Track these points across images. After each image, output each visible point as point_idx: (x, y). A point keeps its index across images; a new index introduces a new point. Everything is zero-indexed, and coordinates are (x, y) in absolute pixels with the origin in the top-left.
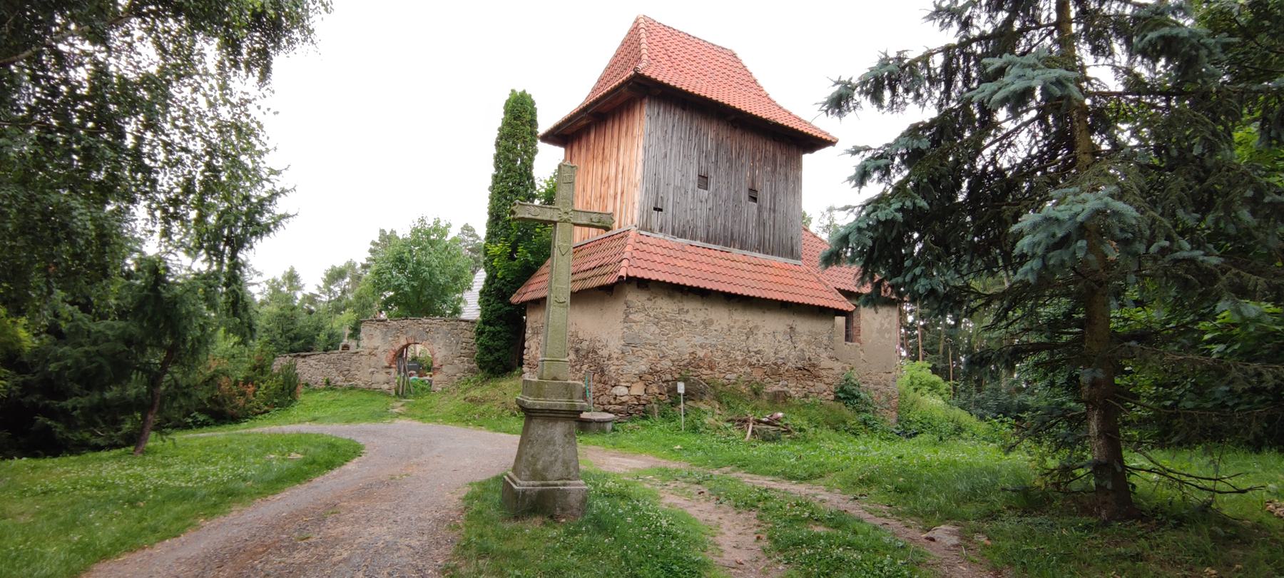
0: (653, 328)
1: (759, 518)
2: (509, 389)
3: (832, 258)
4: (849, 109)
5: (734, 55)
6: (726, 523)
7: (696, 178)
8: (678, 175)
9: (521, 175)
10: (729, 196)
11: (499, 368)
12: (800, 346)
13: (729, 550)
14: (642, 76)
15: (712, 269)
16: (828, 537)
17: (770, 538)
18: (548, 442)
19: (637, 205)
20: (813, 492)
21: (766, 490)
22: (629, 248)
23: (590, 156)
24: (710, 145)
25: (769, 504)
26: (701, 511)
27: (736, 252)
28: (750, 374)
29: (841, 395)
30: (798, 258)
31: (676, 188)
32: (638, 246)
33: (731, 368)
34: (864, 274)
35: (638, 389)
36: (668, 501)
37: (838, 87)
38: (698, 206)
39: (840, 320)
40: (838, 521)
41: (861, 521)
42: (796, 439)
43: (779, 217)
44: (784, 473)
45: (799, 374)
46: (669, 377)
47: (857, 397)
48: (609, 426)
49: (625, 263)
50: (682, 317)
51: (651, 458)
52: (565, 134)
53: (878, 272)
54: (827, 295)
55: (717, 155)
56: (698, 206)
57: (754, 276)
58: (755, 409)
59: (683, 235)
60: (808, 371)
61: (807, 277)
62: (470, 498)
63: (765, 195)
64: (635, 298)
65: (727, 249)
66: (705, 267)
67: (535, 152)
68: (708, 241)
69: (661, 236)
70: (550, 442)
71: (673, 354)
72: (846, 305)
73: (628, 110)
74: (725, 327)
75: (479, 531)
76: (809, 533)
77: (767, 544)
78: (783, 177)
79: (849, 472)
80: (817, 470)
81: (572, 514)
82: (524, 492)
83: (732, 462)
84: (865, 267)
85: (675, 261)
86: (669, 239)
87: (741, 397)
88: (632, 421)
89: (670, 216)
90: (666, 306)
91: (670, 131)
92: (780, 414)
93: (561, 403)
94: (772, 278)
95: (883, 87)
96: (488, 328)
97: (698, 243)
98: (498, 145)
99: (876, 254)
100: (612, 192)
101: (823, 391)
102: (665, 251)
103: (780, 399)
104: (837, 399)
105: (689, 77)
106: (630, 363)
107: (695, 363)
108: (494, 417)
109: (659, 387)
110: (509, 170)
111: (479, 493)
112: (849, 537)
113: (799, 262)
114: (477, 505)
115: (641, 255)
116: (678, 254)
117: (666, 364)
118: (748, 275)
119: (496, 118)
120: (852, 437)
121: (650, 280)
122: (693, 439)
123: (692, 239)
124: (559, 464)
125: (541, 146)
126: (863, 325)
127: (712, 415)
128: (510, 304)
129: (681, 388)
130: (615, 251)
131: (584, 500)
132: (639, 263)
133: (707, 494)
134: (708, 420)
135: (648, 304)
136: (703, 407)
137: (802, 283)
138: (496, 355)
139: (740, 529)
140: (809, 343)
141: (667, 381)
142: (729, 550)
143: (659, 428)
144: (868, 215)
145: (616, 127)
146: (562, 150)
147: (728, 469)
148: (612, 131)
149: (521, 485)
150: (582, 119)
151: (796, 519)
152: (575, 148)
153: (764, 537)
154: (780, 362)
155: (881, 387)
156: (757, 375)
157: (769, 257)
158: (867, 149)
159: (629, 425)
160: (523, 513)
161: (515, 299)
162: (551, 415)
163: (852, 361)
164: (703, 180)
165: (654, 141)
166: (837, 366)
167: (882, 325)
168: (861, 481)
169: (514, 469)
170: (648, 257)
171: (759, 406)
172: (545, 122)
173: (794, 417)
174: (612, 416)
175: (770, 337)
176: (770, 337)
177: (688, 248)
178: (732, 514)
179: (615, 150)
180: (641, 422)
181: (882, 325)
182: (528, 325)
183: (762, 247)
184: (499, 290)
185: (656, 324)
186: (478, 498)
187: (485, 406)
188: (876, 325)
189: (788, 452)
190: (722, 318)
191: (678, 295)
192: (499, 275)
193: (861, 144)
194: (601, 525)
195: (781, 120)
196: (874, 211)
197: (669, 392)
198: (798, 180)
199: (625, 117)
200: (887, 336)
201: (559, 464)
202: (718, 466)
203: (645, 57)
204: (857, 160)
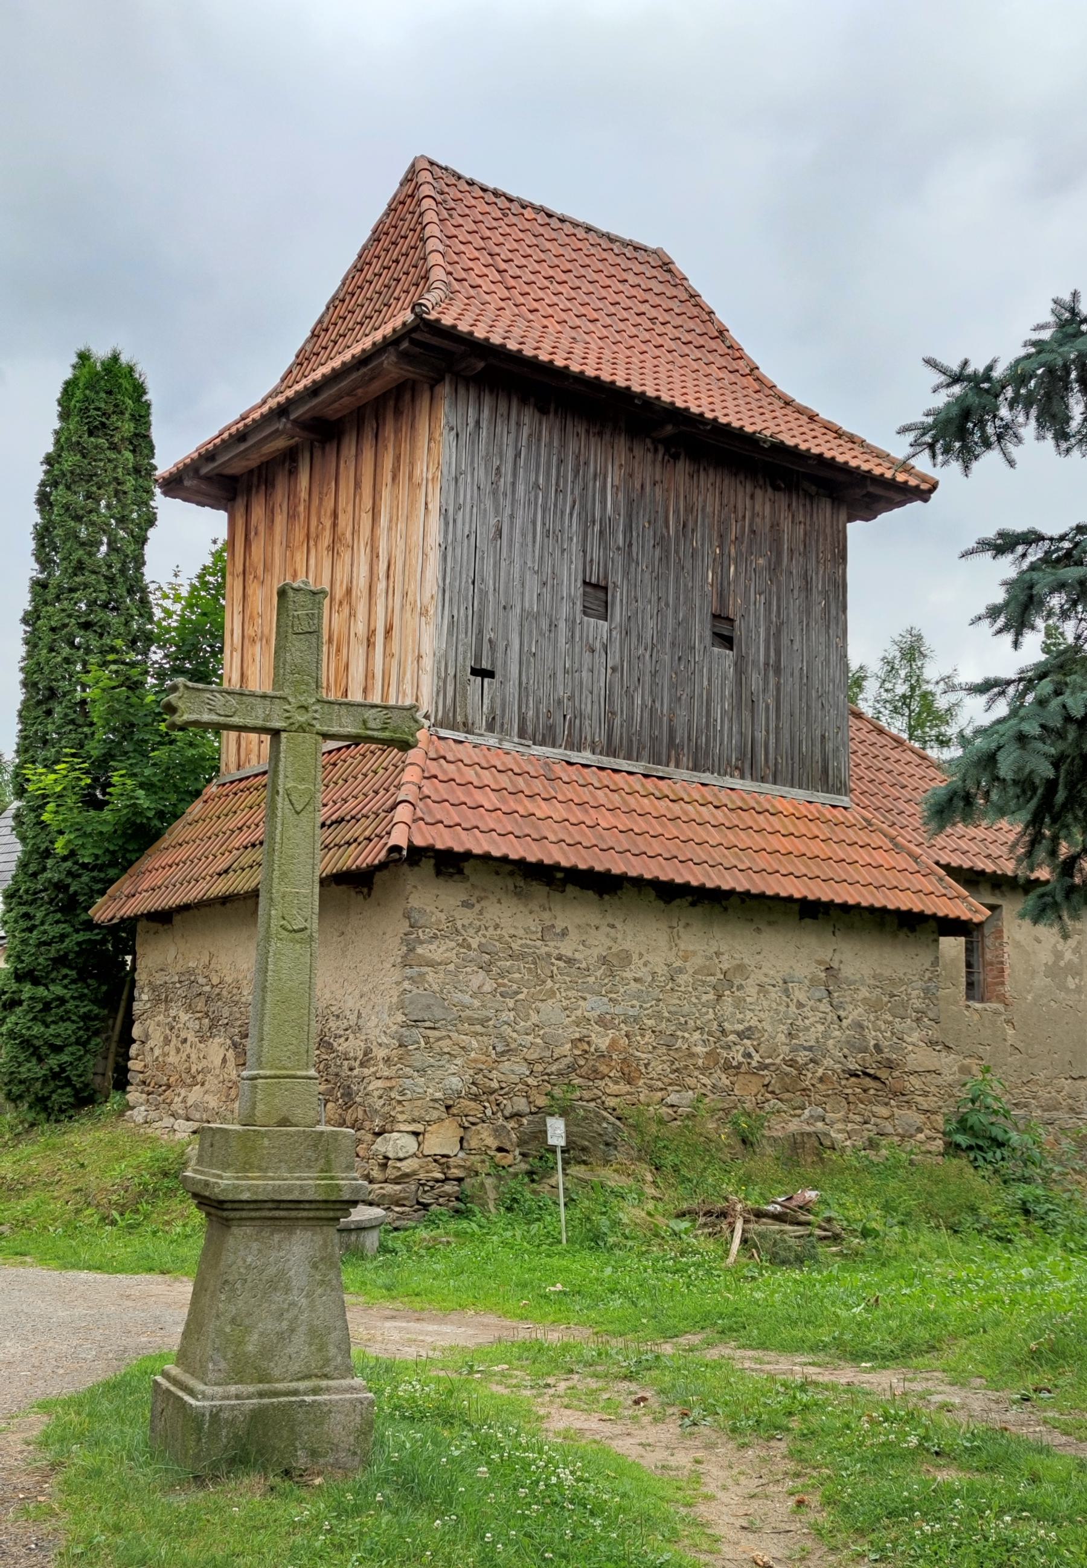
0: (478, 979)
1: (795, 1455)
2: (95, 1150)
3: (953, 806)
4: (987, 444)
5: (666, 265)
6: (715, 1473)
7: (578, 590)
8: (532, 583)
9: (111, 580)
10: (661, 634)
11: (62, 1096)
12: (853, 1014)
13: (732, 1535)
14: (435, 327)
15: (624, 822)
16: (972, 1492)
17: (829, 1501)
18: (273, 1284)
19: (428, 663)
20: (918, 1387)
21: (803, 1388)
22: (411, 775)
23: (299, 534)
24: (611, 503)
25: (817, 1420)
26: (646, 1445)
27: (683, 779)
28: (730, 1091)
29: (961, 1139)
30: (841, 788)
31: (526, 616)
32: (433, 768)
33: (679, 1076)
34: (1034, 843)
35: (442, 1140)
36: (561, 1426)
37: (957, 389)
38: (582, 662)
39: (952, 946)
40: (989, 1453)
41: (1043, 1450)
42: (853, 1257)
43: (790, 685)
44: (838, 1343)
45: (852, 1086)
46: (521, 1104)
47: (1001, 1145)
48: (371, 1240)
49: (403, 813)
50: (551, 947)
51: (491, 1319)
52: (229, 477)
53: (1069, 837)
54: (927, 884)
55: (629, 528)
56: (582, 662)
57: (731, 837)
58: (746, 1180)
59: (548, 738)
60: (875, 1078)
61: (864, 837)
62: (57, 1440)
63: (753, 629)
64: (430, 900)
65: (661, 770)
66: (606, 819)
67: (151, 521)
68: (611, 751)
69: (492, 740)
70: (277, 1283)
71: (532, 1045)
72: (965, 906)
73: (398, 413)
74: (662, 969)
75: (111, 1520)
76: (925, 1484)
77: (825, 1518)
78: (797, 583)
79: (1002, 1333)
80: (922, 1334)
81: (336, 1465)
82: (215, 1416)
83: (703, 1320)
84: (1036, 821)
85: (530, 806)
86: (514, 751)
87: (706, 1149)
88: (432, 1223)
89: (512, 688)
90: (511, 920)
91: (507, 468)
92: (811, 1195)
93: (304, 1183)
94: (775, 843)
95: (1067, 388)
96: (28, 990)
97: (586, 756)
98: (44, 501)
99: (1061, 796)
100: (360, 628)
101: (916, 1129)
102: (504, 780)
103: (807, 1152)
104: (953, 1149)
105: (553, 327)
106: (422, 1071)
107: (588, 1065)
108: (55, 1230)
109: (498, 1132)
110: (80, 567)
111: (77, 1424)
112: (1023, 1489)
113: (845, 800)
114: (81, 1456)
115: (444, 791)
116: (538, 786)
117: (514, 1069)
118: (715, 837)
119: (38, 427)
120: (995, 1247)
121: (468, 855)
122: (588, 1266)
123: (570, 746)
124: (299, 1339)
125: (163, 504)
126: (1010, 955)
127: (638, 1201)
128: (89, 925)
129: (557, 1132)
130: (376, 781)
131: (367, 1428)
132: (438, 812)
133: (654, 1402)
134: (630, 1213)
135: (465, 916)
136: (613, 1179)
137: (853, 854)
138: (53, 1061)
139: (751, 1485)
140: (874, 1007)
141: (517, 1115)
142: (732, 1535)
143: (500, 1238)
144: (1041, 702)
145: (368, 455)
146: (222, 516)
147: (696, 1339)
148: (358, 461)
149: (207, 1396)
150: (276, 433)
151: (889, 1454)
152: (258, 512)
153: (814, 1499)
154: (802, 1057)
155: (1062, 1116)
156: (747, 1091)
157: (766, 787)
158: (1032, 538)
159: (423, 1233)
160: (215, 1466)
161: (103, 911)
162: (280, 1213)
163: (986, 1051)
164: (597, 594)
165: (467, 494)
166: (948, 1063)
167: (1058, 955)
168: (1035, 1355)
169: (183, 1357)
170: (460, 795)
171: (755, 1174)
172: (173, 446)
173: (848, 1200)
174: (377, 1212)
175: (775, 987)
176: (774, 994)
177: (559, 770)
178: (726, 1450)
179: (366, 520)
180: (453, 1226)
181: (1058, 955)
182: (141, 977)
183: (748, 763)
184: (60, 887)
185: (486, 968)
186: (79, 1438)
187: (29, 1202)
188: (1044, 956)
189: (842, 1290)
190: (651, 947)
191: (539, 890)
192: (60, 846)
193: (1019, 527)
194: (414, 1487)
195: (792, 435)
196: (1058, 693)
197: (521, 1143)
198: (837, 591)
199: (389, 430)
200: (1071, 983)
201: (299, 1339)
202: (670, 1334)
203: (437, 274)
204: (1007, 567)
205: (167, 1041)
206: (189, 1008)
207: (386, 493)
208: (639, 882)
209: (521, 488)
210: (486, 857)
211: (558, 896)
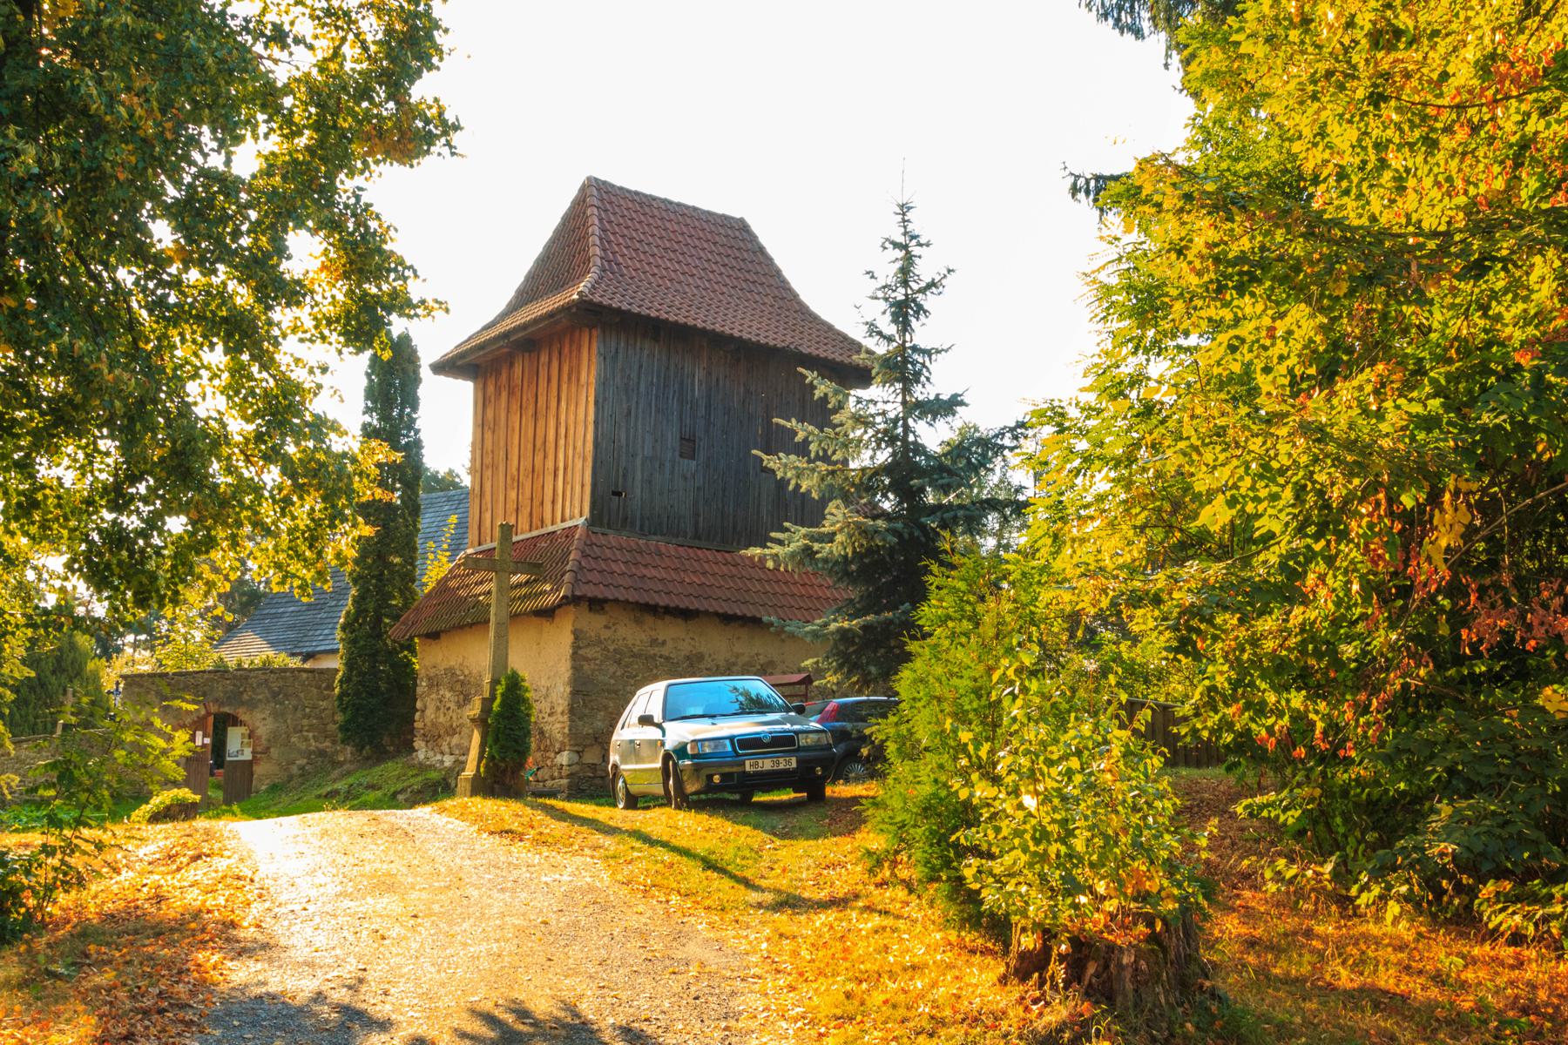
100: (550, 464)
185: (618, 662)
191: (649, 620)
205: (438, 709)
206: (451, 689)
207: (564, 387)
208: (706, 613)
209: (642, 386)
210: (616, 601)
211: (659, 622)
